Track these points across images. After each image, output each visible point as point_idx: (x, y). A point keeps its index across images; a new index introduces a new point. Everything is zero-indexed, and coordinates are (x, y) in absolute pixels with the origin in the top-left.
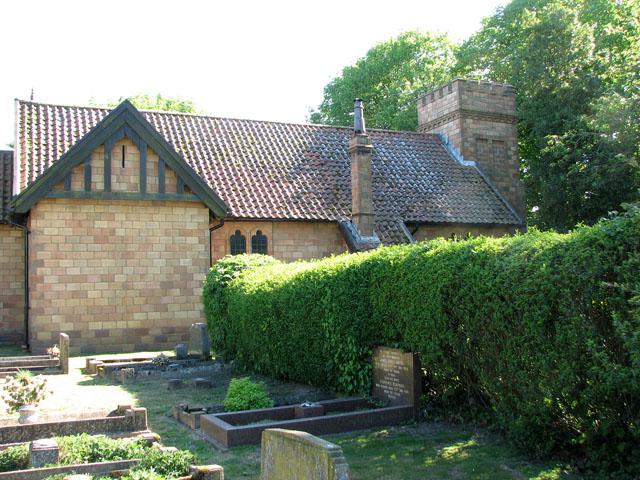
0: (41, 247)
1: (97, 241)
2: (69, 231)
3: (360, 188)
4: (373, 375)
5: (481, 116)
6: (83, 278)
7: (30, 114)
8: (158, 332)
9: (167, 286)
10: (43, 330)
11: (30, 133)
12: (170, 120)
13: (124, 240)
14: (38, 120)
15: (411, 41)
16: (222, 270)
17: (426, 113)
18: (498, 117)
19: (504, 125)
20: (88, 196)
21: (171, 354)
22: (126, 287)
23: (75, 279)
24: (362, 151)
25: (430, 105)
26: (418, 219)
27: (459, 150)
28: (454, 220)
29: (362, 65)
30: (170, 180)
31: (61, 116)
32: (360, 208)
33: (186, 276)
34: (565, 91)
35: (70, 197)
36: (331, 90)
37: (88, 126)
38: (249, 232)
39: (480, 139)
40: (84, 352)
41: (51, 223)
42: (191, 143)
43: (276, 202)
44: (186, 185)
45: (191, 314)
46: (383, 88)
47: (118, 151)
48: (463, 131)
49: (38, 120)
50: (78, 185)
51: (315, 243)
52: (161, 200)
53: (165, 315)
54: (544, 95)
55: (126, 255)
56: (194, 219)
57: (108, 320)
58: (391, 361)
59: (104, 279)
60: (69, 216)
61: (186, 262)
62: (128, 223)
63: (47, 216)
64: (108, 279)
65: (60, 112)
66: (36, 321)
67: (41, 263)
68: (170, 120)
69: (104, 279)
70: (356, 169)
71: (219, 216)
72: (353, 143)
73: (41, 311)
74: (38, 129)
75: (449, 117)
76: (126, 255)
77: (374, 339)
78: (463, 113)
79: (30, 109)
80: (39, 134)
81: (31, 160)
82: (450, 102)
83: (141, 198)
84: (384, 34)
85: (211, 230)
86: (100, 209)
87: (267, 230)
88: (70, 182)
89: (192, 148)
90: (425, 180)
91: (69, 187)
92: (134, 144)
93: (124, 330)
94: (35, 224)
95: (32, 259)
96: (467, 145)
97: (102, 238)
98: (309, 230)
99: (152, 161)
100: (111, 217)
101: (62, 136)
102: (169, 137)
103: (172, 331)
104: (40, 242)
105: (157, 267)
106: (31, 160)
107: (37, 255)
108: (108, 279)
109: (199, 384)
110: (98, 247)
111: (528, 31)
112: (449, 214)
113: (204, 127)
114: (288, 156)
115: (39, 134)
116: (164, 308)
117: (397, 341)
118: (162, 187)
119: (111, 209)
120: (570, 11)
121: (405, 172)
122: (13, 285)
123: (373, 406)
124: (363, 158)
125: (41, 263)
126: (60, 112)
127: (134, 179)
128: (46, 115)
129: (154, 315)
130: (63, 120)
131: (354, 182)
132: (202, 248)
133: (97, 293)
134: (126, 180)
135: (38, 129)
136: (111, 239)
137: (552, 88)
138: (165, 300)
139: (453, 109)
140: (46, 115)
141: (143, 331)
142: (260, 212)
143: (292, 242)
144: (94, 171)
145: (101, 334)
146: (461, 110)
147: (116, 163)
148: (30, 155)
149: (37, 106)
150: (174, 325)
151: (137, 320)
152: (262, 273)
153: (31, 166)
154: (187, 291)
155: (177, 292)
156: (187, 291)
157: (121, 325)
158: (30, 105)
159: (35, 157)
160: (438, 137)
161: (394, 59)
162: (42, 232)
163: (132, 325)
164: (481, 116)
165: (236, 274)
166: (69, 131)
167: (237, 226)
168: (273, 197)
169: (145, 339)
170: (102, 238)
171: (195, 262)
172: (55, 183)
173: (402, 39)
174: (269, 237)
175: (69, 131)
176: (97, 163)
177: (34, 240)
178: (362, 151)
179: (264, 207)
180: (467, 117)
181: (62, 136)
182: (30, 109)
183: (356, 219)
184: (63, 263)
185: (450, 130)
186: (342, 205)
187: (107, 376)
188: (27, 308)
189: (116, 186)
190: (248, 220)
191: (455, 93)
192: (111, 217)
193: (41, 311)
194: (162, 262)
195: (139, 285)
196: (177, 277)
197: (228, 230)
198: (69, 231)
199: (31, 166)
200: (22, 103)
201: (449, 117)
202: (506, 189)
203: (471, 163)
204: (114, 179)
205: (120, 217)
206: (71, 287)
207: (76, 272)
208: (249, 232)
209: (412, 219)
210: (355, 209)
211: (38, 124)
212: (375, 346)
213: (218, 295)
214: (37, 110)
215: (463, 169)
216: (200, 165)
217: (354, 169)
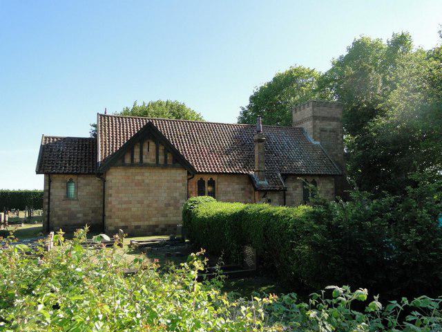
0: (111, 188)
1: (136, 185)
2: (123, 181)
3: (259, 158)
4: (244, 256)
5: (324, 119)
6: (130, 202)
7: (105, 121)
8: (163, 227)
9: (168, 205)
10: (111, 226)
11: (105, 131)
12: (171, 123)
13: (148, 184)
14: (108, 124)
15: (295, 74)
16: (189, 204)
17: (297, 117)
18: (334, 119)
19: (336, 123)
20: (132, 165)
21: (166, 238)
22: (148, 206)
23: (126, 203)
24: (260, 141)
25: (298, 113)
26: (287, 173)
27: (312, 136)
28: (306, 173)
29: (269, 84)
30: (169, 157)
31: (119, 122)
32: (259, 168)
33: (176, 201)
34: (364, 109)
35: (124, 165)
36: (253, 99)
37: (129, 136)
38: (207, 179)
39: (322, 130)
40: (130, 236)
41: (116, 177)
42: (180, 135)
43: (219, 164)
44: (179, 161)
45: (177, 218)
46: (280, 98)
47: (146, 144)
48: (314, 127)
49: (108, 124)
50: (128, 160)
51: (238, 184)
52: (165, 166)
53: (167, 219)
54: (354, 110)
55: (149, 191)
56: (180, 175)
57: (141, 221)
58: (249, 251)
59: (139, 202)
60: (124, 174)
61: (176, 195)
62: (149, 176)
63: (114, 174)
64: (141, 202)
65: (119, 120)
66: (108, 222)
67: (111, 195)
68: (171, 123)
69: (139, 202)
70: (257, 150)
71: (191, 172)
72: (256, 137)
73: (110, 217)
74: (109, 129)
75: (308, 119)
76: (149, 191)
77: (244, 242)
78: (315, 118)
79: (105, 119)
80: (109, 131)
81: (105, 145)
82: (308, 112)
83: (157, 165)
84: (283, 68)
85: (188, 179)
86: (138, 171)
87: (215, 178)
88: (124, 158)
89: (181, 138)
90: (293, 152)
91: (123, 161)
92: (153, 141)
93: (148, 226)
94: (108, 178)
95: (106, 193)
96: (315, 133)
97: (138, 184)
98: (235, 179)
99: (161, 148)
100: (143, 175)
101: (120, 132)
102: (168, 137)
103: (169, 226)
104: (110, 193)
105: (163, 197)
106: (105, 145)
107: (108, 191)
108: (141, 202)
109: (177, 255)
110: (136, 188)
111: (348, 77)
112: (303, 170)
113: (187, 126)
114: (226, 143)
115: (109, 131)
116: (165, 215)
117: (250, 243)
118: (166, 160)
119: (143, 171)
120: (370, 67)
121: (283, 148)
122: (96, 203)
123: (242, 269)
124: (261, 144)
125: (111, 195)
126: (119, 120)
127: (154, 157)
128: (112, 121)
129: (163, 219)
130: (120, 124)
131: (256, 155)
132: (184, 188)
133: (136, 209)
134: (149, 158)
135: (109, 129)
136: (143, 184)
137: (358, 107)
138: (167, 212)
139: (309, 116)
140: (112, 121)
141: (156, 226)
142: (211, 170)
143: (226, 183)
144: (135, 153)
145: (138, 227)
146: (314, 117)
147: (145, 150)
148: (105, 142)
149: (108, 117)
150: (169, 223)
151: (153, 222)
152: (208, 207)
153: (105, 148)
154: (177, 208)
155: (172, 208)
156: (177, 208)
157: (146, 223)
158: (104, 116)
159: (107, 143)
160: (302, 129)
161: (284, 84)
162: (111, 181)
163: (151, 223)
164: (324, 119)
165: (196, 206)
166: (123, 130)
167: (201, 176)
168: (218, 162)
169: (157, 230)
170: (138, 184)
171: (180, 194)
172: (118, 158)
173: (291, 72)
174: (216, 181)
175: (123, 130)
176: (137, 150)
177: (107, 185)
178: (260, 141)
179: (214, 167)
180: (316, 119)
181: (120, 132)
182: (105, 119)
183: (257, 173)
184: (120, 195)
185: (308, 126)
186: (251, 166)
187: (139, 249)
188: (104, 215)
189: (145, 160)
190: (206, 173)
191: (311, 108)
192: (143, 175)
193: (110, 217)
194: (165, 195)
195: (155, 205)
196: (172, 201)
197: (197, 178)
198: (123, 181)
199: (105, 148)
200: (101, 115)
201: (308, 119)
202: (336, 155)
203: (318, 143)
204: (144, 157)
205: (147, 174)
206: (124, 206)
207: (126, 199)
208: (207, 179)
209: (284, 172)
210: (256, 169)
211: (108, 126)
212: (244, 245)
213: (188, 214)
214: (108, 119)
215: (313, 146)
216: (183, 148)
217: (256, 149)
